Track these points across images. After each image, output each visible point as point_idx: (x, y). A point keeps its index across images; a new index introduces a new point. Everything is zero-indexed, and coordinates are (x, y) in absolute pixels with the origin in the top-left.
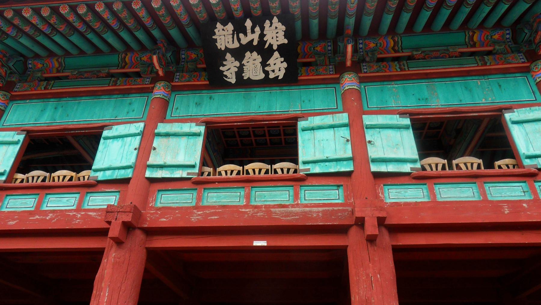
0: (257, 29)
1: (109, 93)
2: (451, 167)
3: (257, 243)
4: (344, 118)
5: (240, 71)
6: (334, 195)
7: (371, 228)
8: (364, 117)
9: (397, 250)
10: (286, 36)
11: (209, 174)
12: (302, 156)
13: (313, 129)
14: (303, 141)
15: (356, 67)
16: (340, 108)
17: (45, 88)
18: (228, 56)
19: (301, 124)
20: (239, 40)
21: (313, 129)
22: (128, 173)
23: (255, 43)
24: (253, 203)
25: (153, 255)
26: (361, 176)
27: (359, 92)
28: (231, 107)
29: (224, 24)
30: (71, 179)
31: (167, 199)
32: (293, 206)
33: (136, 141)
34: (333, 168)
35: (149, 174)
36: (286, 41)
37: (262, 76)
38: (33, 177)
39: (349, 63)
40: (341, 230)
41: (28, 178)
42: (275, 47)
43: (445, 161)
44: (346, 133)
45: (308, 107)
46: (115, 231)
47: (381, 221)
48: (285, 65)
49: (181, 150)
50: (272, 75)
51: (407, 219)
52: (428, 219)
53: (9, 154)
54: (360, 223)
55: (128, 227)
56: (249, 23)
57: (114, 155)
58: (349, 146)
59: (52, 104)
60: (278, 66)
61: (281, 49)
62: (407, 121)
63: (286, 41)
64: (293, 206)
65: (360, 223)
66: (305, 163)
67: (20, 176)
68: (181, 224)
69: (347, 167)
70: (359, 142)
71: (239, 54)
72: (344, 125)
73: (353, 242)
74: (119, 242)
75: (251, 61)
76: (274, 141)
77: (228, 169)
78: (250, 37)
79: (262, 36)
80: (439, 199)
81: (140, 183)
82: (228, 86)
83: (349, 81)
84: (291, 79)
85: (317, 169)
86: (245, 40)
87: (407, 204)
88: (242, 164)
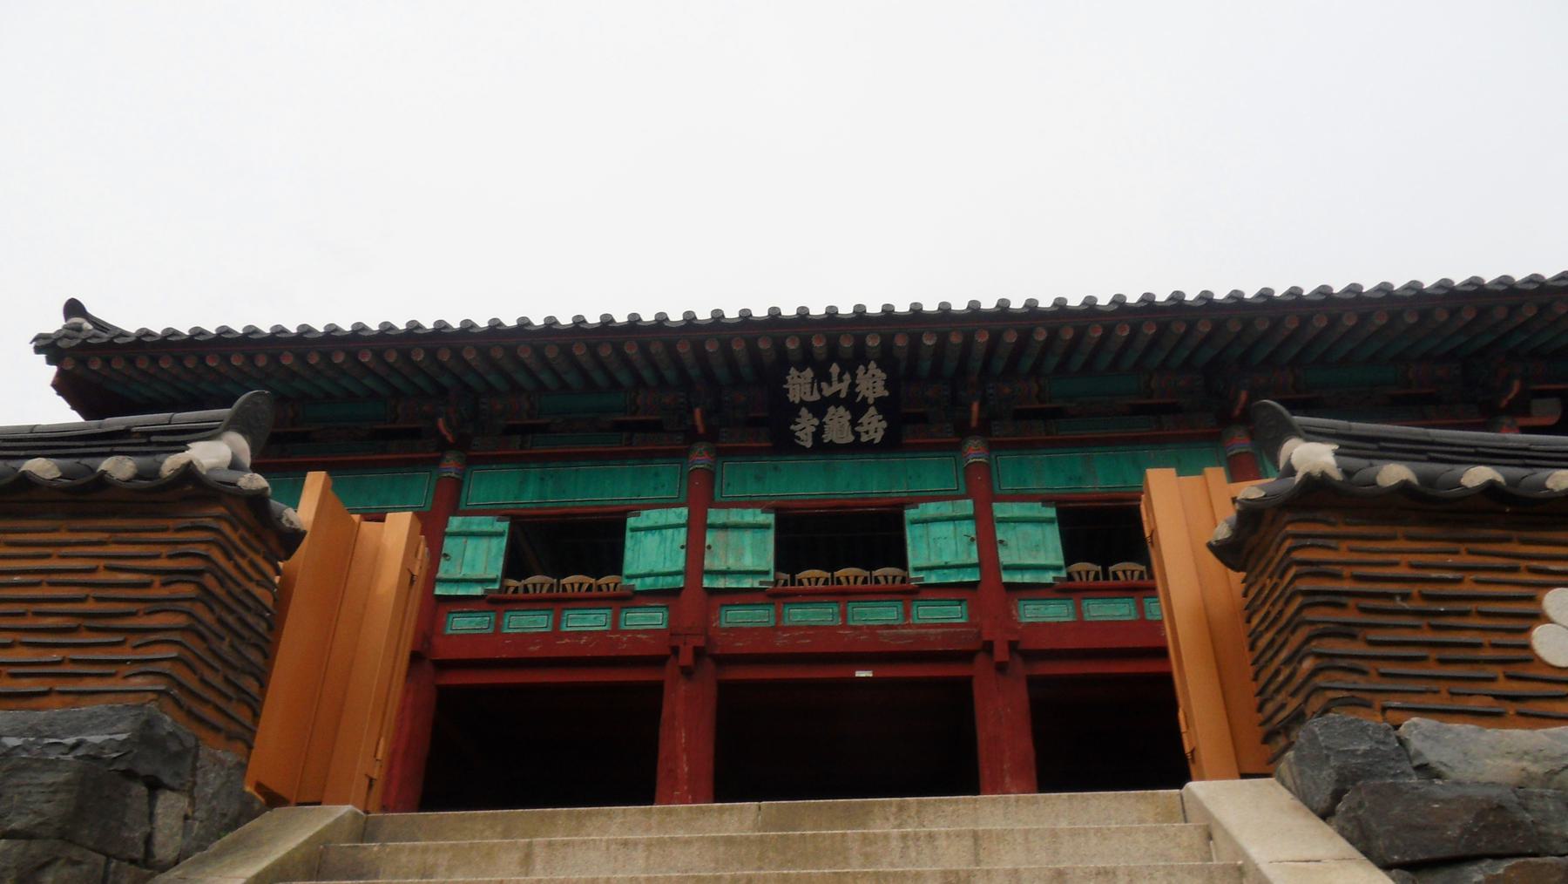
0: (847, 377)
1: (621, 457)
2: (1106, 577)
3: (861, 674)
4: (967, 507)
5: (819, 431)
6: (955, 613)
7: (1001, 654)
8: (995, 505)
9: (1032, 682)
10: (886, 386)
11: (785, 584)
12: (912, 562)
13: (925, 521)
14: (913, 539)
15: (984, 429)
16: (963, 491)
17: (522, 447)
18: (804, 411)
19: (910, 514)
20: (820, 390)
21: (925, 521)
22: (679, 582)
23: (843, 395)
24: (851, 623)
25: (727, 692)
26: (989, 588)
27: (987, 467)
28: (808, 484)
29: (801, 370)
30: (590, 588)
31: (735, 616)
32: (903, 627)
33: (681, 536)
34: (953, 577)
35: (439, 591)
36: (886, 394)
37: (851, 438)
38: (534, 585)
39: (974, 423)
40: (966, 656)
41: (526, 587)
42: (871, 401)
43: (1143, 568)
44: (969, 528)
45: (916, 487)
46: (686, 658)
47: (1013, 646)
48: (884, 424)
49: (745, 551)
50: (864, 438)
51: (1047, 644)
52: (1070, 643)
53: (494, 550)
54: (988, 647)
55: (699, 653)
56: (835, 369)
57: (653, 551)
58: (974, 548)
59: (534, 471)
60: (874, 426)
61: (880, 403)
62: (1051, 512)
63: (886, 394)
64: (903, 627)
65: (988, 647)
66: (917, 569)
67: (512, 583)
68: (764, 649)
69: (972, 576)
70: (987, 542)
71: (818, 409)
72: (966, 518)
73: (980, 671)
74: (687, 672)
75: (836, 418)
76: (872, 537)
77: (811, 576)
78: (836, 387)
79: (853, 385)
80: (1087, 617)
81: (690, 595)
82: (802, 451)
83: (975, 452)
84: (892, 444)
85: (933, 579)
86: (828, 391)
87: (1045, 624)
88: (832, 568)
